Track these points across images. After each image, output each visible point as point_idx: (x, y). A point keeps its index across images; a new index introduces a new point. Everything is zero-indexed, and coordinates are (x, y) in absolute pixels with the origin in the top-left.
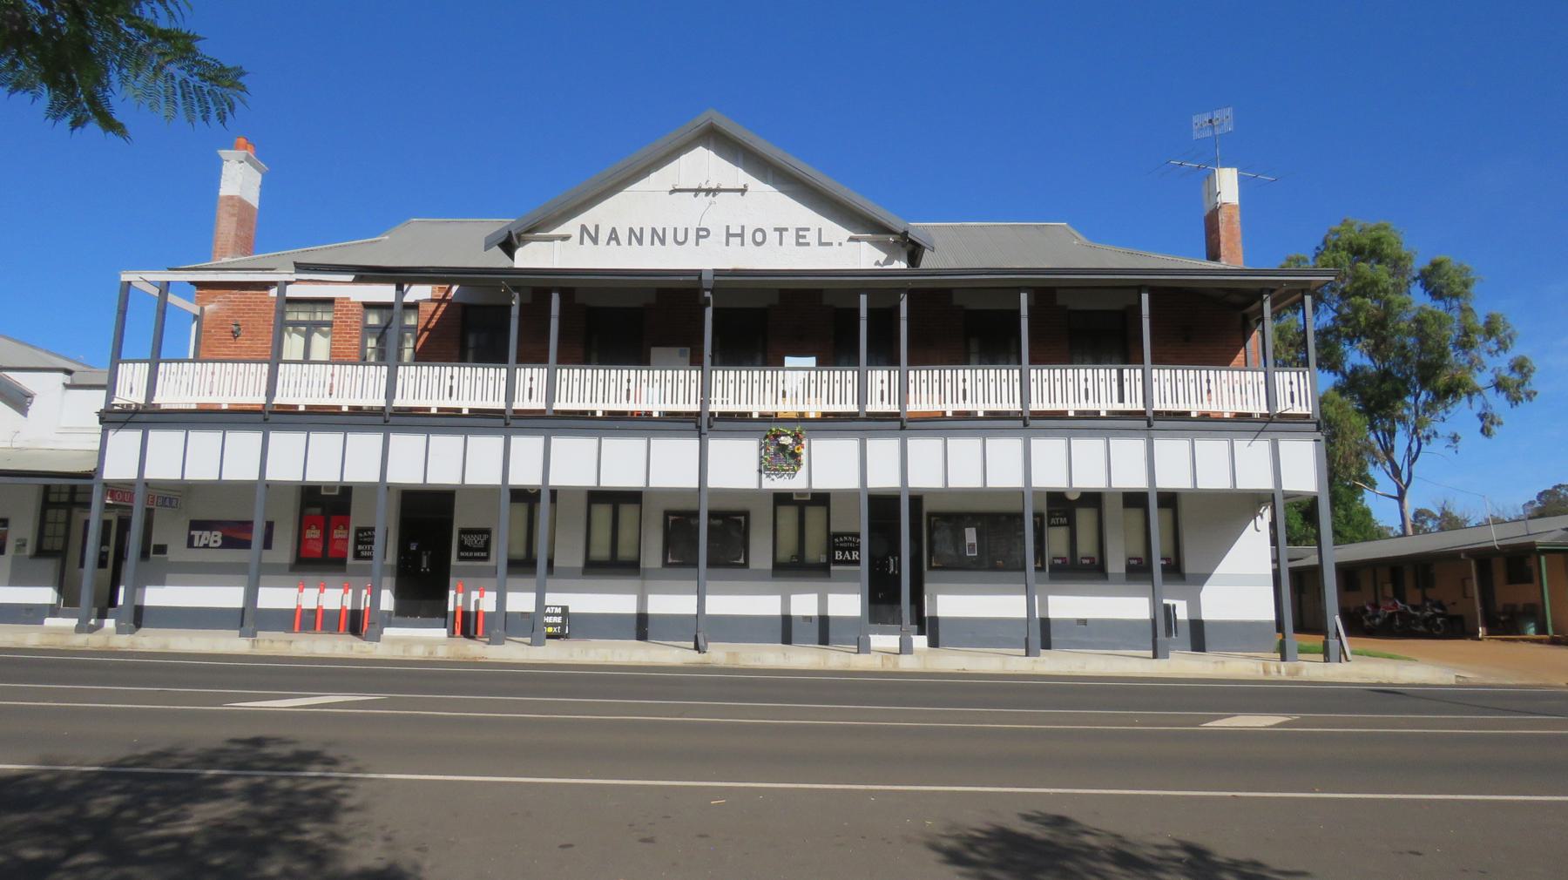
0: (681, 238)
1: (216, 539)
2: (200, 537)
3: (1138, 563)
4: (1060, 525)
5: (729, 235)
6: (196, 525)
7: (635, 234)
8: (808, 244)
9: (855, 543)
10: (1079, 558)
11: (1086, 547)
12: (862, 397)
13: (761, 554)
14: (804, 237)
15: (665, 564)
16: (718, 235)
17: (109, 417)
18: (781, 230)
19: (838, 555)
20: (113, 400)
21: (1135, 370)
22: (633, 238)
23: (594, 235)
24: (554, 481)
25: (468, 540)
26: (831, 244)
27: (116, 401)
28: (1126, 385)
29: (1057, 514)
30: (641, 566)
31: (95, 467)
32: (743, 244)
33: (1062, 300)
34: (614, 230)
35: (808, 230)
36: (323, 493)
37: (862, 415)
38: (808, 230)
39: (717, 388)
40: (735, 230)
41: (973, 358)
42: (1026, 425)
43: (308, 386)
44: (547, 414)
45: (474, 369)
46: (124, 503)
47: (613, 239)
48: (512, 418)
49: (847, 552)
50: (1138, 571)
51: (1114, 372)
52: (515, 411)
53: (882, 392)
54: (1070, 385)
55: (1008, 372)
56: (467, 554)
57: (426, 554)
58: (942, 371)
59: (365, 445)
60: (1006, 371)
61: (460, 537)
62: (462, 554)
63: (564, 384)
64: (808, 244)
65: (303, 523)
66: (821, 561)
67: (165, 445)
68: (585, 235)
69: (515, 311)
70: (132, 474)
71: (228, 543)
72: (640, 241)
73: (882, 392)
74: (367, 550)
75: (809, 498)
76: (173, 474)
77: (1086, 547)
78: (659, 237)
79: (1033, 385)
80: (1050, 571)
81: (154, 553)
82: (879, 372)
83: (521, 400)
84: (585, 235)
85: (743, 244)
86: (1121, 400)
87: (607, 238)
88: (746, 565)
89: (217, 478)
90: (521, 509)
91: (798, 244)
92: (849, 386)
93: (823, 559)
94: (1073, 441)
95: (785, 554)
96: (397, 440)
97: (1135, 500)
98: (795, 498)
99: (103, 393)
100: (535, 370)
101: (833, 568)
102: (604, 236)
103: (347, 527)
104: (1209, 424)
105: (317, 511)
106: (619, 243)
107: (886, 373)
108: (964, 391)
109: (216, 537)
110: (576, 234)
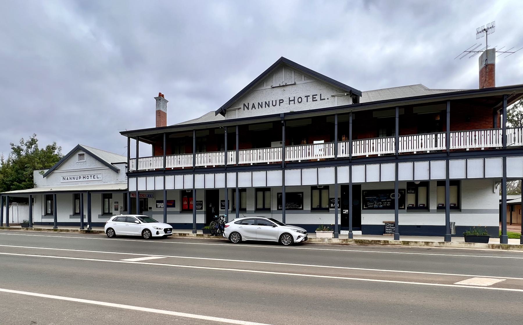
0: (274, 104)
4: (411, 193)
5: (290, 101)
7: (260, 104)
8: (317, 100)
10: (419, 204)
11: (422, 201)
12: (336, 153)
13: (307, 207)
14: (315, 98)
15: (278, 209)
16: (286, 101)
18: (307, 97)
20: (129, 170)
21: (487, 131)
22: (259, 106)
24: (139, 190)
26: (325, 99)
27: (130, 170)
28: (439, 140)
29: (411, 189)
30: (271, 210)
32: (294, 103)
33: (416, 111)
35: (317, 95)
36: (187, 192)
38: (317, 95)
39: (287, 154)
41: (293, 144)
45: (212, 153)
47: (253, 107)
48: (450, 153)
50: (441, 208)
51: (434, 136)
52: (228, 165)
53: (343, 150)
54: (415, 142)
55: (390, 139)
58: (365, 141)
62: (222, 207)
63: (241, 156)
64: (317, 100)
66: (327, 207)
68: (245, 107)
69: (237, 133)
72: (262, 107)
73: (343, 150)
77: (453, 200)
78: (267, 104)
80: (407, 209)
84: (245, 107)
85: (294, 103)
86: (436, 146)
88: (302, 209)
91: (313, 101)
92: (331, 149)
94: (468, 160)
97: (441, 183)
100: (233, 152)
102: (250, 107)
105: (186, 196)
106: (255, 108)
108: (373, 147)
110: (242, 106)
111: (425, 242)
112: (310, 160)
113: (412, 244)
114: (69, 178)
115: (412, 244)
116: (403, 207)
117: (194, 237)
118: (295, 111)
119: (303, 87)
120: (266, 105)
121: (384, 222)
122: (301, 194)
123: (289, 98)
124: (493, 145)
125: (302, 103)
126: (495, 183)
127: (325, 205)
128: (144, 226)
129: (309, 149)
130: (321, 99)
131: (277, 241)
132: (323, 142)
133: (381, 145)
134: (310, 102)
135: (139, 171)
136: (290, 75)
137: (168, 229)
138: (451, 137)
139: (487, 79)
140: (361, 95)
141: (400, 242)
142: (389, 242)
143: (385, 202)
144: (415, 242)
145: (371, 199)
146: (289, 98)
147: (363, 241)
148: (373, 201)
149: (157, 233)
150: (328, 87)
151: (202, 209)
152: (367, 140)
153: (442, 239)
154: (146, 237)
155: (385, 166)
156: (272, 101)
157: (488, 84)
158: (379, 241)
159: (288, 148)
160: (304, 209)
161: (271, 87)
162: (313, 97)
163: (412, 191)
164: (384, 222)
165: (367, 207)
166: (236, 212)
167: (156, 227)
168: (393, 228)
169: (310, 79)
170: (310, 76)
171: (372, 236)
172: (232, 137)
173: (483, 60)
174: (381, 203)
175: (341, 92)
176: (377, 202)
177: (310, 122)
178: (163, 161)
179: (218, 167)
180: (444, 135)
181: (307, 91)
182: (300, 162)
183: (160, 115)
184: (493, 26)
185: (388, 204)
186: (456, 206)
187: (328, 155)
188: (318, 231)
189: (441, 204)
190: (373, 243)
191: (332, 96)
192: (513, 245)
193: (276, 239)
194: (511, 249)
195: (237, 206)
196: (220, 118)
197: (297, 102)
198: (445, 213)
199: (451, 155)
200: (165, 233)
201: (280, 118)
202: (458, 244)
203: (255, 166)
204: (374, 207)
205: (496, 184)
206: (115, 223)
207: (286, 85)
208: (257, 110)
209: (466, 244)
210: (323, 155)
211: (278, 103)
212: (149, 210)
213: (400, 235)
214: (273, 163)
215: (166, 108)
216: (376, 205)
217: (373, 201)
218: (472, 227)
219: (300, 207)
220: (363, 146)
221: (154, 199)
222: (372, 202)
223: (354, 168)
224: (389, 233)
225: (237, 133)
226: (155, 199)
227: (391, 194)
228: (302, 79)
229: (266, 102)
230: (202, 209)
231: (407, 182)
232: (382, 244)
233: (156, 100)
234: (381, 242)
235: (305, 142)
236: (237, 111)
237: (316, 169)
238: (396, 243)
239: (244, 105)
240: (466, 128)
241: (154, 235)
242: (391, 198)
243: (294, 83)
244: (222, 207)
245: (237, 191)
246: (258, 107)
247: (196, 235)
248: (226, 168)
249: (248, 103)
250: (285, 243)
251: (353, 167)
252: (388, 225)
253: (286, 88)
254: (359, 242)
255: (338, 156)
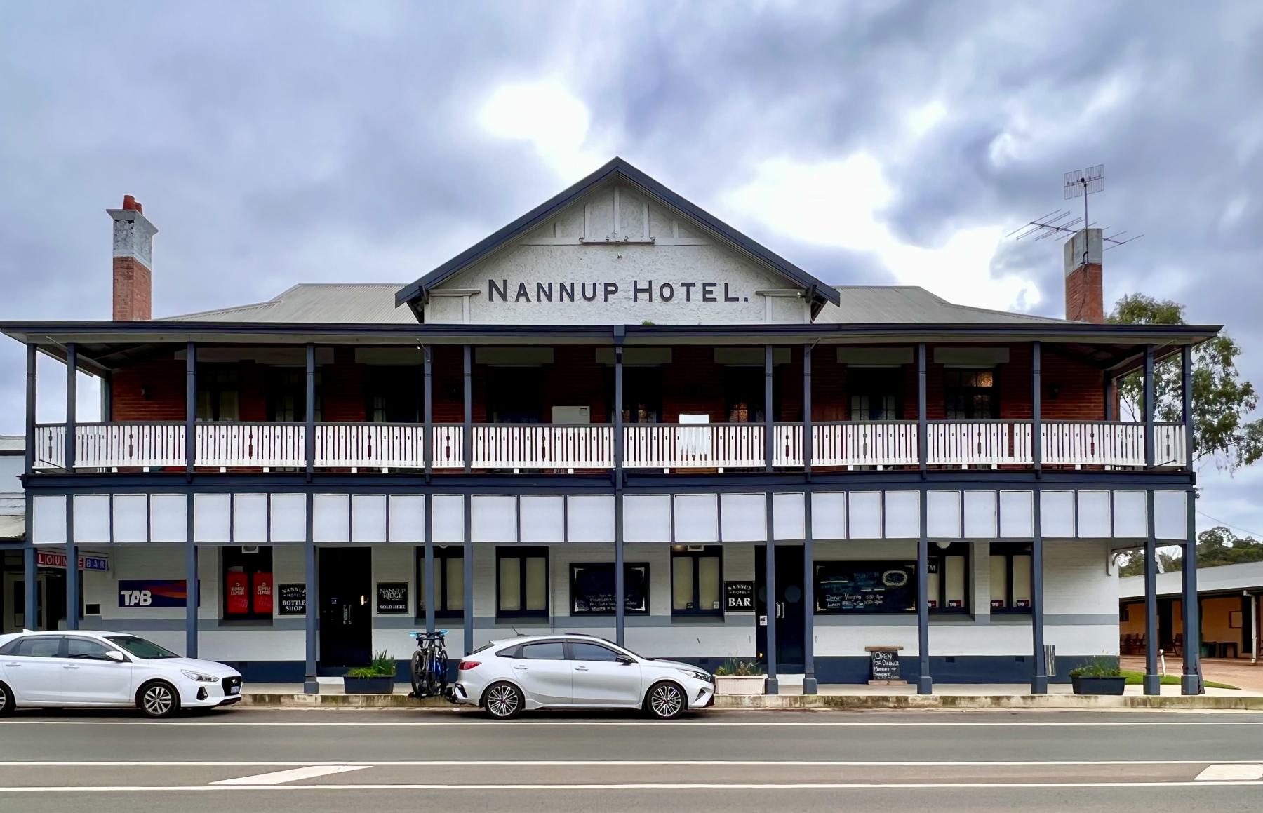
0: (589, 294)
1: (145, 598)
2: (130, 596)
3: (1000, 605)
5: (637, 291)
6: (124, 585)
8: (714, 300)
9: (302, 593)
10: (947, 600)
12: (768, 455)
13: (660, 604)
14: (711, 292)
15: (573, 613)
16: (626, 290)
17: (1187, 479)
18: (688, 285)
19: (732, 602)
22: (542, 294)
23: (494, 289)
24: (78, 539)
25: (389, 594)
26: (737, 299)
28: (1016, 439)
30: (550, 615)
31: (24, 532)
32: (651, 300)
34: (522, 286)
35: (714, 285)
36: (244, 552)
37: (769, 471)
38: (714, 285)
40: (643, 285)
41: (378, 415)
42: (1038, 478)
43: (100, 447)
44: (767, 471)
46: (56, 567)
47: (523, 295)
48: (813, 475)
49: (739, 599)
50: (1005, 611)
51: (1006, 426)
53: (787, 447)
56: (386, 607)
57: (347, 608)
59: (289, 507)
60: (506, 429)
61: (378, 591)
62: (382, 607)
64: (714, 300)
65: (226, 583)
66: (715, 607)
67: (89, 507)
68: (494, 291)
69: (428, 369)
70: (61, 539)
71: (156, 603)
72: (549, 297)
73: (787, 447)
74: (291, 605)
75: (702, 550)
76: (874, 533)
77: (954, 594)
78: (567, 292)
79: (930, 440)
81: (87, 613)
82: (784, 428)
83: (1160, 457)
84: (494, 291)
85: (651, 300)
86: (1011, 454)
87: (516, 294)
88: (647, 612)
89: (108, 541)
90: (1000, 560)
91: (705, 299)
92: (756, 442)
93: (716, 606)
94: (569, 498)
95: (682, 603)
96: (80, 501)
98: (689, 550)
99: (22, 459)
101: (726, 614)
102: (513, 291)
103: (270, 585)
104: (1094, 478)
105: (240, 568)
106: (528, 300)
107: (790, 429)
109: (145, 597)
110: (484, 288)
111: (991, 697)
112: (330, 469)
113: (963, 702)
114: (532, 291)
115: (963, 702)
116: (914, 609)
117: (315, 707)
118: (657, 322)
119: (676, 255)
120: (564, 294)
121: (867, 649)
122: (643, 569)
123: (635, 282)
124: (1116, 460)
125: (673, 301)
126: (1109, 552)
127: (708, 601)
128: (147, 670)
129: (543, 438)
130: (727, 299)
131: (639, 706)
132: (705, 419)
133: (853, 440)
134: (697, 302)
135: (77, 472)
136: (635, 214)
137: (234, 681)
138: (422, 438)
139: (1088, 300)
140: (839, 302)
141: (936, 700)
142: (910, 701)
143: (869, 593)
144: (969, 697)
145: (835, 586)
146: (635, 282)
147: (845, 699)
148: (841, 591)
149: (201, 694)
150: (746, 266)
151: (405, 611)
152: (983, 423)
153: (1026, 690)
154: (155, 710)
155: (243, 500)
156: (584, 284)
157: (1089, 311)
158: (885, 699)
159: (631, 430)
160: (653, 612)
161: (580, 243)
162: (606, 289)
163: (931, 566)
164: (867, 649)
165: (826, 607)
166: (463, 623)
167: (192, 672)
168: (891, 664)
169: (695, 236)
170: (696, 228)
171: (852, 688)
172: (788, 378)
173: (1076, 252)
174: (859, 597)
175: (781, 286)
176: (850, 595)
177: (549, 358)
178: (183, 441)
179: (900, 470)
180: (1029, 427)
181: (688, 269)
182: (146, 473)
183: (130, 277)
184: (1100, 176)
185: (878, 600)
186: (937, 606)
187: (484, 460)
188: (722, 674)
189: (1021, 601)
190: (870, 703)
191: (758, 293)
192: (1172, 698)
193: (634, 701)
194: (1168, 707)
195: (432, 604)
196: (406, 316)
197: (659, 298)
198: (1031, 622)
199: (1045, 478)
200: (226, 694)
201: (612, 339)
202: (1064, 698)
203: (890, 473)
204: (844, 608)
205: (1112, 553)
206: (14, 662)
207: (626, 244)
208: (535, 305)
209: (1080, 699)
210: (709, 457)
211: (600, 291)
212: (85, 614)
213: (818, 683)
214: (555, 472)
215: (150, 252)
216: (846, 603)
217: (841, 591)
218: (1089, 658)
219: (640, 606)
220: (838, 440)
221: (109, 575)
222: (838, 595)
223: (320, 500)
224: (880, 679)
225: (428, 369)
226: (114, 574)
227: (885, 574)
228: (672, 232)
229: (562, 285)
230: (405, 611)
231: (756, 547)
232: (892, 705)
233: (112, 221)
234: (889, 701)
235: (744, 414)
236: (466, 299)
237: (345, 498)
238: (926, 703)
239: (492, 284)
240: (1049, 414)
241: (189, 699)
242: (884, 584)
243: (650, 241)
244: (382, 607)
245: (429, 553)
246: (536, 298)
247: (320, 700)
248: (312, 478)
249: (505, 282)
250: (662, 712)
251: (930, 494)
252: (878, 655)
253: (627, 252)
254: (835, 704)
255: (775, 464)
